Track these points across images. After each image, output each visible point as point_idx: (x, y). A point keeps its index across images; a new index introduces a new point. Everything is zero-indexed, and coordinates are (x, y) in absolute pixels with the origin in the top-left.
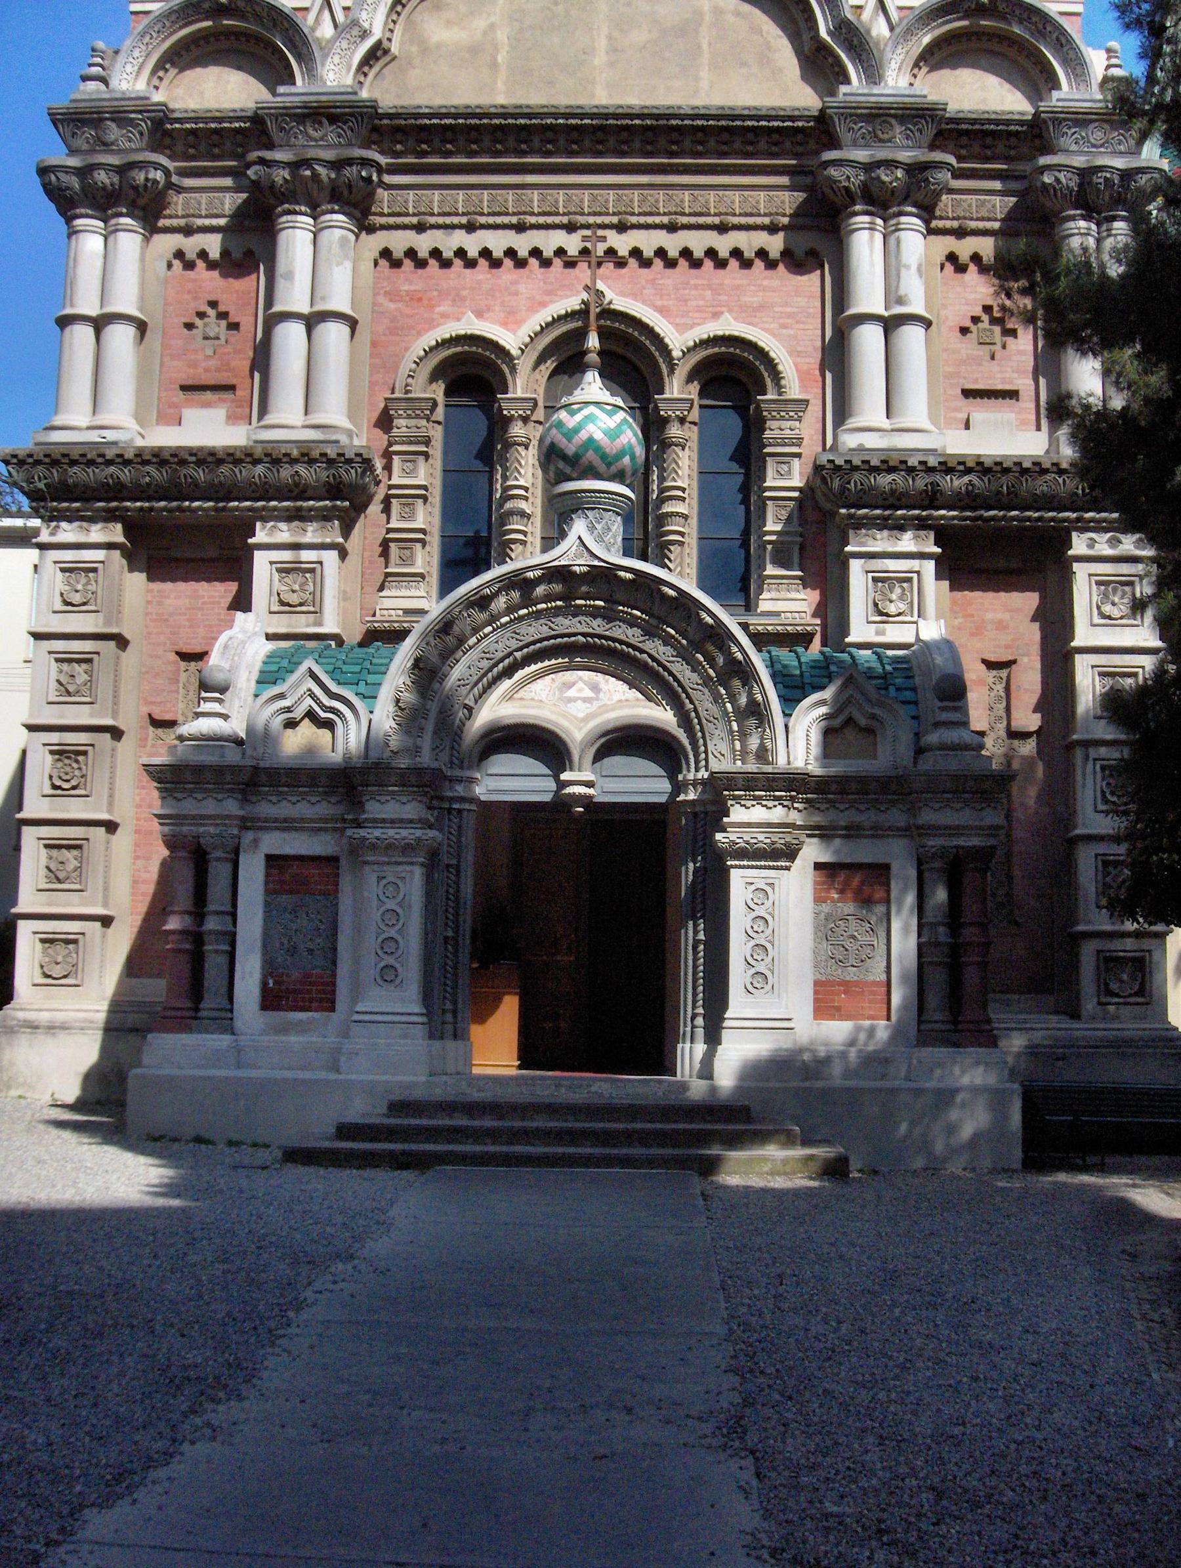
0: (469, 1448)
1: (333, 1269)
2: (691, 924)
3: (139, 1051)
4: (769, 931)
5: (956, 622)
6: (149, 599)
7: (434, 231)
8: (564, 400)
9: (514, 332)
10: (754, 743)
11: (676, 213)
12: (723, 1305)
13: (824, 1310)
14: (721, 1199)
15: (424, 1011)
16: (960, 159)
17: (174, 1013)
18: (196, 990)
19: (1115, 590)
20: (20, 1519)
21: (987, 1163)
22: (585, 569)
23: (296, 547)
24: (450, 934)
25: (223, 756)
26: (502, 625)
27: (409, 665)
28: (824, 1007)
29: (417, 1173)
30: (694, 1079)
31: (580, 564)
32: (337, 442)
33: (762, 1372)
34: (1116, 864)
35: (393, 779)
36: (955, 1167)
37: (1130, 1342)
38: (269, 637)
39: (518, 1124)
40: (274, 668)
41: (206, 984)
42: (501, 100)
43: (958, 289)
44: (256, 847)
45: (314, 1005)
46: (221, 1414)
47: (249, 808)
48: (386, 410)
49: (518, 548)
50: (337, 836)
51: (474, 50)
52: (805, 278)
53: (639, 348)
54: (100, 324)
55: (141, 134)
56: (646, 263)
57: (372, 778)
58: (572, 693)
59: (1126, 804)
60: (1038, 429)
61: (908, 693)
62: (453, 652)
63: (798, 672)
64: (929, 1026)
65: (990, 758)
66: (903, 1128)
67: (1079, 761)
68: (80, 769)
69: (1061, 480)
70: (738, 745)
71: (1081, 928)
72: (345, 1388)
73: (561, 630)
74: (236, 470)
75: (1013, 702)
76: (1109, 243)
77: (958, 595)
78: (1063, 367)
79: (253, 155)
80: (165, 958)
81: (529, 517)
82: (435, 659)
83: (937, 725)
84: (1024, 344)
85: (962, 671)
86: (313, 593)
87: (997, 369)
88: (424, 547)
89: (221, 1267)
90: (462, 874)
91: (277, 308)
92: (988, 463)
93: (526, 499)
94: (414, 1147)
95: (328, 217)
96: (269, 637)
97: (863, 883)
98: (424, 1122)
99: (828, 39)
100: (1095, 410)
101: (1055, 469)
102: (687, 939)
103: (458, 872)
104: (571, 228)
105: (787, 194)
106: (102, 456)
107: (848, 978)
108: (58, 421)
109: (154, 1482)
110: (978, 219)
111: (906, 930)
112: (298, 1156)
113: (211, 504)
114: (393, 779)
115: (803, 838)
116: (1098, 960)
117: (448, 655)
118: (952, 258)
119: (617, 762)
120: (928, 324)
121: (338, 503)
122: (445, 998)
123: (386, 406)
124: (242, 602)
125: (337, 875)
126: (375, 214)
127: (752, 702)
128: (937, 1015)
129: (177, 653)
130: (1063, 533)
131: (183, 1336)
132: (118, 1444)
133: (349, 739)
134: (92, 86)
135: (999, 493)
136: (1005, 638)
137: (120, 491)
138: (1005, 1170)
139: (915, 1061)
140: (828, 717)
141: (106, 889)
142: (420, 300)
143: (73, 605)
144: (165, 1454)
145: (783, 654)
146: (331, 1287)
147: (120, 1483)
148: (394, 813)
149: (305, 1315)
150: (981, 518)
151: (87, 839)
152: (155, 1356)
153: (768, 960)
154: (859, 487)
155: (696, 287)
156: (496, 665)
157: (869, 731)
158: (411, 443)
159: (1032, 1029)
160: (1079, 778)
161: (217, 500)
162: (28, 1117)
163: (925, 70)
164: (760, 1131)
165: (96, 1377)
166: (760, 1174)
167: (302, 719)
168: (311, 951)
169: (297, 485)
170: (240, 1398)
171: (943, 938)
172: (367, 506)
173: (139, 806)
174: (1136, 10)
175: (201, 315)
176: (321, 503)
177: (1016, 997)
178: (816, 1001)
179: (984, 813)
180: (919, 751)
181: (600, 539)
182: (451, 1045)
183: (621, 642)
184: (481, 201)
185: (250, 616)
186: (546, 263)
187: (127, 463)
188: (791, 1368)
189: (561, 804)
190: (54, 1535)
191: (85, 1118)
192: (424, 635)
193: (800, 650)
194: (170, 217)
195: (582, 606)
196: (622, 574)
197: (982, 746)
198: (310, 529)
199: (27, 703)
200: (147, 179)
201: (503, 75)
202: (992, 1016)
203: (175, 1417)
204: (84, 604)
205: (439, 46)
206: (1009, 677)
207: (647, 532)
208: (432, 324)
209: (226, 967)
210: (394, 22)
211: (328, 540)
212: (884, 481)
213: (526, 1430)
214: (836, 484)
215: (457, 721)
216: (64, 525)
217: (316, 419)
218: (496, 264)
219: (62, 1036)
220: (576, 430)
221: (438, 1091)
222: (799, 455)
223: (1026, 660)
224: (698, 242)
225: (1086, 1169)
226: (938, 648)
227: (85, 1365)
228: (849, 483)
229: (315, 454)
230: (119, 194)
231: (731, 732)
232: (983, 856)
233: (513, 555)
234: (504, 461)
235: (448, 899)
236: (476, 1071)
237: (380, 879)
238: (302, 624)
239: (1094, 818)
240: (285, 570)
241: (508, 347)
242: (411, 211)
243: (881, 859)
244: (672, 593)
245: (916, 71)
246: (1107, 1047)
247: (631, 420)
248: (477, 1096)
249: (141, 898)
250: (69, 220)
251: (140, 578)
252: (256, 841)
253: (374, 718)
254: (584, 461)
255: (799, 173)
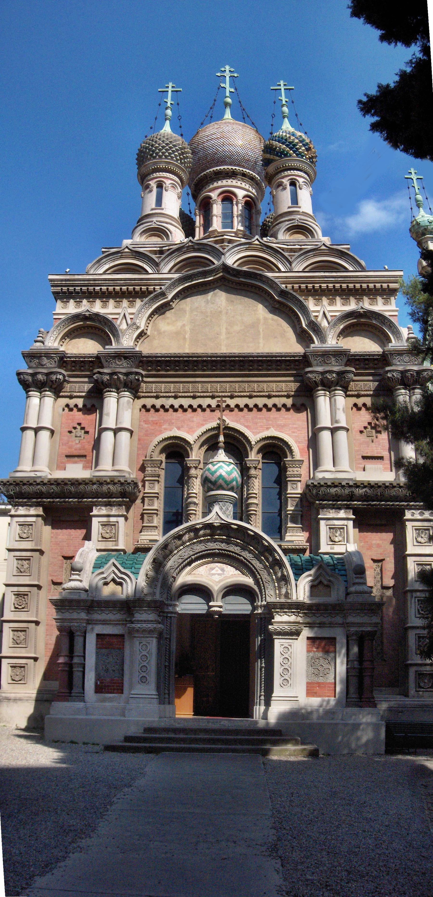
0: (175, 856)
1: (124, 790)
2: (259, 660)
3: (49, 709)
4: (289, 663)
5: (361, 544)
6: (52, 536)
7: (162, 399)
8: (211, 460)
9: (192, 435)
10: (284, 591)
11: (252, 391)
12: (270, 804)
13: (308, 806)
14: (270, 765)
15: (157, 694)
16: (356, 369)
17: (62, 694)
18: (70, 685)
19: (422, 532)
20: (12, 880)
21: (371, 752)
22: (219, 524)
23: (109, 516)
24: (167, 664)
25: (80, 596)
26: (187, 546)
27: (151, 561)
28: (310, 692)
29: (155, 755)
30: (260, 720)
31: (217, 522)
32: (124, 476)
33: (284, 829)
34: (423, 637)
35: (145, 605)
36: (359, 753)
37: (423, 818)
38: (98, 550)
39: (193, 736)
40: (100, 562)
41: (74, 683)
42: (187, 351)
43: (358, 417)
44: (93, 631)
45: (115, 691)
46: (83, 843)
47: (90, 616)
48: (143, 465)
49: (193, 516)
50: (124, 627)
51: (178, 333)
52: (301, 414)
53: (239, 441)
54: (37, 430)
55: (55, 362)
56: (241, 410)
57: (137, 604)
58: (213, 572)
59: (427, 614)
60: (391, 471)
61: (343, 572)
62: (168, 556)
63: (300, 564)
64: (350, 700)
65: (374, 597)
66: (340, 738)
67: (409, 598)
68: (25, 601)
69: (400, 490)
70: (277, 592)
71: (409, 662)
72: (129, 834)
73: (209, 548)
74: (86, 487)
75: (384, 575)
76: (414, 398)
77: (362, 534)
78: (400, 448)
79: (96, 371)
80: (58, 673)
81: (197, 504)
82: (161, 559)
83: (354, 584)
84: (384, 437)
85: (364, 563)
86: (115, 534)
87: (374, 446)
88: (157, 516)
89: (82, 789)
90: (172, 641)
91: (103, 426)
92: (372, 484)
93: (196, 498)
94: (154, 745)
95: (123, 393)
96: (98, 550)
97: (325, 645)
98: (157, 735)
99: (306, 328)
100: (413, 464)
101: (398, 486)
102: (258, 666)
103: (170, 640)
104: (213, 397)
105: (293, 384)
106: (35, 482)
107: (320, 681)
108: (19, 469)
109: (60, 867)
110: (364, 391)
111: (342, 663)
112: (110, 748)
113: (76, 500)
114: (145, 605)
115: (303, 627)
116: (416, 674)
117: (166, 557)
118: (355, 405)
119: (231, 598)
120: (347, 430)
121: (125, 499)
122: (165, 688)
123: (143, 463)
124: (88, 537)
125: (124, 642)
126: (140, 392)
127: (283, 575)
128: (354, 695)
129: (63, 557)
130: (402, 510)
131: (68, 815)
132: (46, 853)
133: (128, 589)
134: (38, 344)
135: (377, 495)
136: (380, 551)
137: (42, 495)
138: (378, 754)
139: (345, 713)
140: (312, 581)
141: (35, 647)
142: (157, 423)
143: (23, 538)
144: (63, 857)
145: (295, 557)
146: (123, 797)
147: (47, 867)
148: (145, 617)
149: (113, 807)
150: (370, 505)
151: (28, 628)
152: (58, 822)
153: (289, 674)
154: (323, 493)
155: (260, 418)
156: (184, 561)
157: (328, 586)
158: (152, 477)
159: (390, 701)
160: (409, 604)
161: (79, 498)
162: (7, 734)
163: (342, 337)
164: (285, 739)
165: (37, 830)
166: (285, 755)
167: (110, 582)
168: (114, 671)
169: (109, 493)
170: (90, 837)
171: (356, 666)
172: (135, 501)
173: (48, 615)
174: (417, 315)
175: (75, 428)
176: (118, 500)
177: (384, 688)
178: (307, 690)
179: (373, 618)
180: (347, 594)
181: (224, 513)
182: (167, 707)
183: (233, 552)
184: (180, 388)
185: (91, 542)
186: (204, 410)
187: (45, 484)
188: (295, 827)
189: (209, 615)
190: (24, 886)
191: (29, 734)
192: (157, 550)
193: (301, 555)
194: (65, 392)
195: (217, 538)
196: (233, 526)
197: (371, 592)
198: (114, 509)
199: (5, 576)
200: (56, 378)
201: (187, 343)
202: (375, 696)
203: (67, 844)
204: (27, 538)
205: (164, 332)
206: (382, 565)
207: (242, 511)
208: (161, 432)
209: (81, 677)
210: (149, 323)
211: (121, 513)
212: (333, 490)
213: (197, 849)
214: (314, 492)
215: (170, 583)
216: (20, 508)
217: (117, 468)
218: (185, 410)
219: (19, 703)
220: (215, 472)
221: (163, 724)
222: (300, 481)
223: (388, 559)
224: (260, 402)
225: (409, 754)
226: (355, 555)
227: (32, 825)
228: (319, 491)
229: (116, 481)
230: (46, 384)
231: (275, 587)
232: (372, 635)
233: (191, 519)
234: (188, 483)
235: (166, 651)
236: (177, 716)
237: (140, 643)
238: (110, 546)
239: (415, 620)
240: (104, 525)
241: (189, 441)
242: (154, 391)
243: (332, 635)
244: (252, 533)
245: (338, 338)
246: (419, 708)
247: (236, 468)
248: (177, 726)
249: (48, 650)
250: (27, 392)
251: (49, 528)
252: (92, 629)
253: (137, 582)
254: (218, 483)
255: (298, 376)
